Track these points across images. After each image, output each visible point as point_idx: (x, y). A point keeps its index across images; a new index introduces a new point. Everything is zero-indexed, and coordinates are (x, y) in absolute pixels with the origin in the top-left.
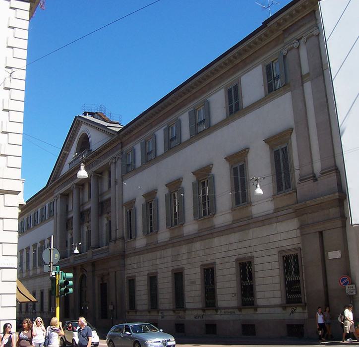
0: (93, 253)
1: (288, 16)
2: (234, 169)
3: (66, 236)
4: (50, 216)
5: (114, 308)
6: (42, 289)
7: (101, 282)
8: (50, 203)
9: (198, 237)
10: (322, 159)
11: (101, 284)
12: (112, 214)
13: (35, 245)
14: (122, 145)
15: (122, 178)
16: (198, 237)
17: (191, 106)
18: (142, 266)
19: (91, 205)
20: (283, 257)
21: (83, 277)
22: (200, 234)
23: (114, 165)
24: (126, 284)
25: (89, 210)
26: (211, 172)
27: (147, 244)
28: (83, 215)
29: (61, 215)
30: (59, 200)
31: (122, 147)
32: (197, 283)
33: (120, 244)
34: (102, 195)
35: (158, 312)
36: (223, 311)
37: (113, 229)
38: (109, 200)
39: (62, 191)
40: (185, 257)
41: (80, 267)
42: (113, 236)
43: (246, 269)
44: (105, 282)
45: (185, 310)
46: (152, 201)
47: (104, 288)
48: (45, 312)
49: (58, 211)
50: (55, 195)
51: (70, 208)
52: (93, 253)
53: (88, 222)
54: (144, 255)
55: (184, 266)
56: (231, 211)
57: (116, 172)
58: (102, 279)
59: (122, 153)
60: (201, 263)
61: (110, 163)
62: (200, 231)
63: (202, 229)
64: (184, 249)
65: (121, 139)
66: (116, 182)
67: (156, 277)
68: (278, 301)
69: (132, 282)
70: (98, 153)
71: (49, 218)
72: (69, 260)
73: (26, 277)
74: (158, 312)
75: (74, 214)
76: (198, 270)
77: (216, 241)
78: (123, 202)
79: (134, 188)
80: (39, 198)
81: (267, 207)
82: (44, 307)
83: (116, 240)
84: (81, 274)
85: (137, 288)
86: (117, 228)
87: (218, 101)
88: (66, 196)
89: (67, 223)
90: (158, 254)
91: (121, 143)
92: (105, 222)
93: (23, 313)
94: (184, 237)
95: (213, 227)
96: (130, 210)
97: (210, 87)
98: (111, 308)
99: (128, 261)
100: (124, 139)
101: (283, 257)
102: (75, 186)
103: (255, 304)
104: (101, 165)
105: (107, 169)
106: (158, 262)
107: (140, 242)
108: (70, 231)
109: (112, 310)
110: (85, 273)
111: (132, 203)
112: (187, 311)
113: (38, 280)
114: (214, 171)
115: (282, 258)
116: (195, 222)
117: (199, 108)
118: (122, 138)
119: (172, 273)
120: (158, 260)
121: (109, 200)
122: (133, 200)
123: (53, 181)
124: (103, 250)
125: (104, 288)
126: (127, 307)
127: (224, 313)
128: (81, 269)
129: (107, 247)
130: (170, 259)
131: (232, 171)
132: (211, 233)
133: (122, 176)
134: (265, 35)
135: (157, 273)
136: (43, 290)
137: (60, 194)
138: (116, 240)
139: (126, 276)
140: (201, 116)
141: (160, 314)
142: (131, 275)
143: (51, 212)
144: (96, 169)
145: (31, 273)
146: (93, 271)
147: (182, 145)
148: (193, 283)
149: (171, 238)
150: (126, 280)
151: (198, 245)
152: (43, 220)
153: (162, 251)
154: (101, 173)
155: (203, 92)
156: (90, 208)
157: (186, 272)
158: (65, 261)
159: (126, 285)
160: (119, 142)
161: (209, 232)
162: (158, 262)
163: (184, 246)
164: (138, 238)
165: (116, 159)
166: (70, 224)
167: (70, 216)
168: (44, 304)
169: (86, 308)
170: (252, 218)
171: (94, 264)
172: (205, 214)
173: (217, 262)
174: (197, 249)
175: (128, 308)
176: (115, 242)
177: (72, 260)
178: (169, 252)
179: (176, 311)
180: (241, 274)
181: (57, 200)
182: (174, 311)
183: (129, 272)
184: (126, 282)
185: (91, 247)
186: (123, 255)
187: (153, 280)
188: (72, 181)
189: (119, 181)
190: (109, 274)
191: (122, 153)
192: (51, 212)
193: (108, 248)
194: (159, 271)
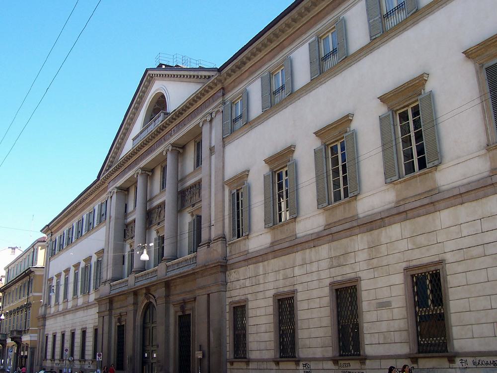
0: (167, 267)
1: (310, 4)
2: (487, 69)
3: (123, 249)
4: (100, 222)
5: (203, 356)
6: (84, 326)
7: (180, 314)
8: (61, 236)
9: (274, 252)
10: (113, 271)
11: (180, 316)
12: (204, 203)
13: (77, 266)
14: (224, 91)
15: (224, 142)
16: (274, 252)
17: (310, 36)
18: (262, 281)
19: (167, 197)
20: (412, 276)
21: (149, 306)
22: (402, 209)
23: (208, 125)
24: (227, 315)
25: (162, 206)
26: (349, 127)
27: (272, 243)
28: (151, 216)
29: (116, 218)
30: (114, 197)
31: (224, 95)
32: (394, 305)
33: (218, 247)
34: (183, 180)
35: (297, 362)
36: (470, 360)
37: (204, 225)
38: (198, 185)
39: (120, 182)
40: (362, 256)
41: (144, 291)
42: (204, 236)
43: (346, 297)
44: (187, 312)
45: (363, 359)
46: (343, 138)
47: (185, 324)
48: (88, 360)
49: (113, 214)
50: (110, 190)
51: (131, 208)
52: (167, 267)
53: (132, 238)
54: (266, 263)
55: (360, 274)
56: (484, 151)
57: (212, 135)
58: (183, 308)
59: (51, 240)
60: (404, 265)
61: (201, 124)
62: (402, 203)
63: (275, 241)
64: (360, 242)
65: (218, 82)
66: (212, 150)
67: (244, 306)
68: (329, 353)
69: (240, 311)
70: (180, 112)
71: (98, 225)
72: (127, 281)
73: (54, 313)
74: (297, 362)
75: (136, 215)
76: (399, 279)
77: (445, 217)
78: (223, 179)
79: (246, 155)
80: (77, 206)
81: (477, 168)
82: (86, 353)
83: (208, 244)
84: (146, 301)
85: (251, 322)
86: (213, 222)
87: (301, 57)
88: (124, 191)
89: (125, 230)
90: (298, 257)
91: (223, 88)
92: (187, 219)
93: (56, 362)
94: (359, 218)
95: (434, 191)
96: (237, 190)
97: (293, 39)
98: (199, 355)
99: (233, 275)
100: (229, 80)
101: (412, 276)
102: (140, 171)
103: (362, 353)
104: (186, 131)
105: (196, 138)
106: (297, 271)
107: (259, 239)
108: (129, 241)
109: (200, 359)
110: (153, 301)
111: (243, 176)
112: (367, 362)
113: (80, 314)
114: (296, 155)
115: (409, 278)
116: (266, 230)
117: (236, 101)
118: (225, 79)
119: (331, 290)
120: (296, 268)
121: (198, 185)
122: (245, 172)
123: (107, 170)
124: (186, 260)
125: (185, 324)
126: (229, 354)
127: (474, 363)
128: (146, 294)
129: (193, 255)
130: (324, 264)
131: (484, 75)
132: (432, 203)
133: (223, 138)
134: (274, 34)
135: (294, 292)
136: (86, 328)
137: (116, 187)
138: (208, 244)
139: (228, 301)
140: (278, 82)
141: (301, 367)
142: (237, 299)
143: (102, 216)
144: (175, 140)
145: (70, 305)
146: (167, 296)
147: (293, 95)
148: (384, 305)
149: (328, 226)
150: (228, 307)
151: (395, 231)
152: (90, 228)
153: (308, 251)
154: (184, 147)
155: (281, 47)
156: (164, 203)
157: (364, 285)
158: (120, 283)
159: (228, 317)
160: (219, 86)
161: (426, 201)
162: (297, 271)
163: (359, 236)
164: (253, 235)
165: (214, 115)
166: (130, 231)
167: (130, 219)
168: (87, 348)
169: (152, 355)
170: (248, 253)
171: (168, 284)
172: (337, 197)
173: (449, 257)
174: (394, 239)
175: (232, 357)
176: (209, 246)
177: (131, 280)
178: (324, 251)
179: (342, 362)
180: (416, 294)
181: (111, 197)
182: (335, 361)
183: (236, 294)
184: (228, 310)
185: (133, 270)
186: (224, 266)
187: (285, 307)
188: (136, 164)
189: (218, 148)
190: (195, 298)
191: (224, 103)
192: (102, 216)
193: (195, 257)
194: (299, 288)
